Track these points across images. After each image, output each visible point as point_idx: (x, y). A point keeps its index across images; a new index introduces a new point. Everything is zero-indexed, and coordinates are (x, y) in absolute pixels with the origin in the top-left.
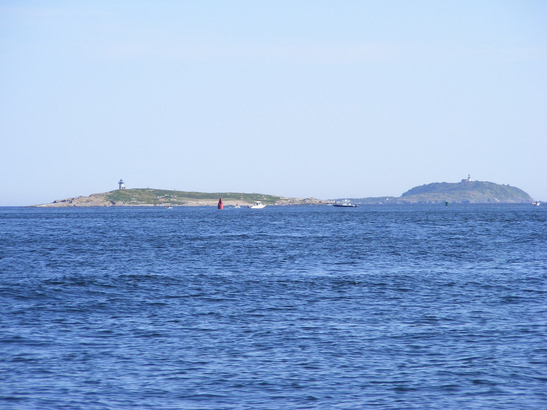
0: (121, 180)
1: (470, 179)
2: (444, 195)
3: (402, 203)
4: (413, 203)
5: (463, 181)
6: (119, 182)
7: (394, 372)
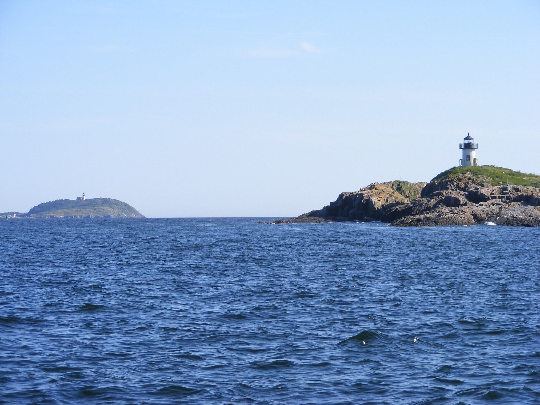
0: (467, 138)
1: (84, 197)
2: (85, 210)
3: (50, 218)
4: (60, 218)
5: (78, 198)
6: (463, 142)
7: (83, 300)
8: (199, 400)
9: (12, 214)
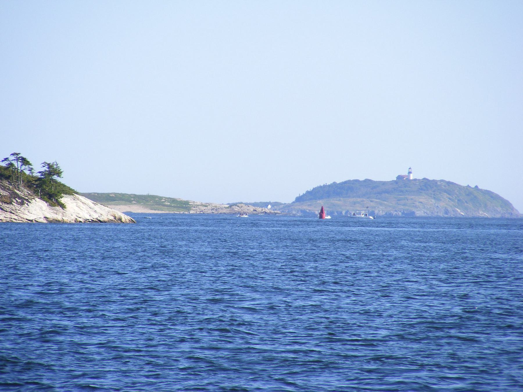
1: (411, 175)
2: (371, 201)
5: (400, 177)
8: (480, 367)
9: (266, 204)
